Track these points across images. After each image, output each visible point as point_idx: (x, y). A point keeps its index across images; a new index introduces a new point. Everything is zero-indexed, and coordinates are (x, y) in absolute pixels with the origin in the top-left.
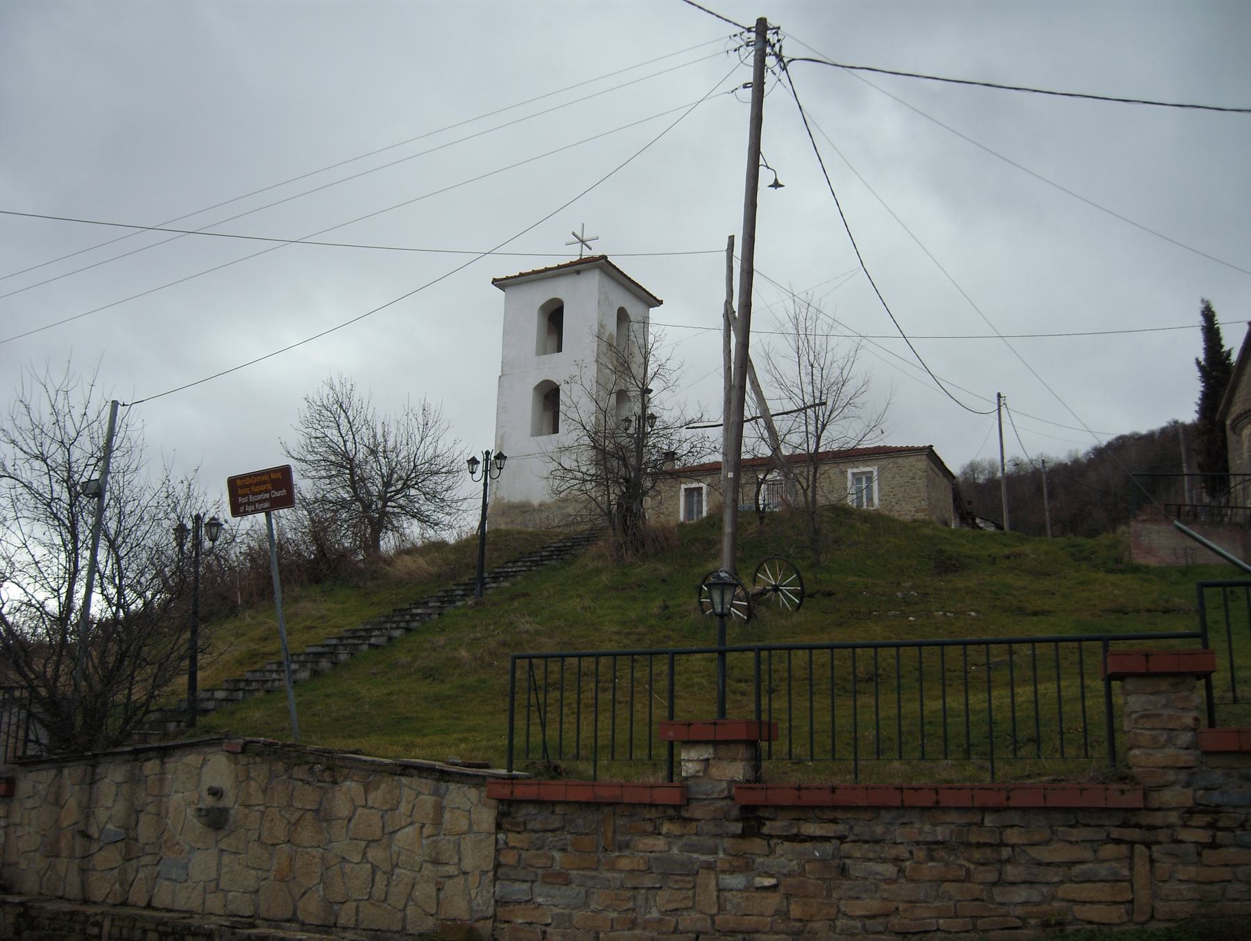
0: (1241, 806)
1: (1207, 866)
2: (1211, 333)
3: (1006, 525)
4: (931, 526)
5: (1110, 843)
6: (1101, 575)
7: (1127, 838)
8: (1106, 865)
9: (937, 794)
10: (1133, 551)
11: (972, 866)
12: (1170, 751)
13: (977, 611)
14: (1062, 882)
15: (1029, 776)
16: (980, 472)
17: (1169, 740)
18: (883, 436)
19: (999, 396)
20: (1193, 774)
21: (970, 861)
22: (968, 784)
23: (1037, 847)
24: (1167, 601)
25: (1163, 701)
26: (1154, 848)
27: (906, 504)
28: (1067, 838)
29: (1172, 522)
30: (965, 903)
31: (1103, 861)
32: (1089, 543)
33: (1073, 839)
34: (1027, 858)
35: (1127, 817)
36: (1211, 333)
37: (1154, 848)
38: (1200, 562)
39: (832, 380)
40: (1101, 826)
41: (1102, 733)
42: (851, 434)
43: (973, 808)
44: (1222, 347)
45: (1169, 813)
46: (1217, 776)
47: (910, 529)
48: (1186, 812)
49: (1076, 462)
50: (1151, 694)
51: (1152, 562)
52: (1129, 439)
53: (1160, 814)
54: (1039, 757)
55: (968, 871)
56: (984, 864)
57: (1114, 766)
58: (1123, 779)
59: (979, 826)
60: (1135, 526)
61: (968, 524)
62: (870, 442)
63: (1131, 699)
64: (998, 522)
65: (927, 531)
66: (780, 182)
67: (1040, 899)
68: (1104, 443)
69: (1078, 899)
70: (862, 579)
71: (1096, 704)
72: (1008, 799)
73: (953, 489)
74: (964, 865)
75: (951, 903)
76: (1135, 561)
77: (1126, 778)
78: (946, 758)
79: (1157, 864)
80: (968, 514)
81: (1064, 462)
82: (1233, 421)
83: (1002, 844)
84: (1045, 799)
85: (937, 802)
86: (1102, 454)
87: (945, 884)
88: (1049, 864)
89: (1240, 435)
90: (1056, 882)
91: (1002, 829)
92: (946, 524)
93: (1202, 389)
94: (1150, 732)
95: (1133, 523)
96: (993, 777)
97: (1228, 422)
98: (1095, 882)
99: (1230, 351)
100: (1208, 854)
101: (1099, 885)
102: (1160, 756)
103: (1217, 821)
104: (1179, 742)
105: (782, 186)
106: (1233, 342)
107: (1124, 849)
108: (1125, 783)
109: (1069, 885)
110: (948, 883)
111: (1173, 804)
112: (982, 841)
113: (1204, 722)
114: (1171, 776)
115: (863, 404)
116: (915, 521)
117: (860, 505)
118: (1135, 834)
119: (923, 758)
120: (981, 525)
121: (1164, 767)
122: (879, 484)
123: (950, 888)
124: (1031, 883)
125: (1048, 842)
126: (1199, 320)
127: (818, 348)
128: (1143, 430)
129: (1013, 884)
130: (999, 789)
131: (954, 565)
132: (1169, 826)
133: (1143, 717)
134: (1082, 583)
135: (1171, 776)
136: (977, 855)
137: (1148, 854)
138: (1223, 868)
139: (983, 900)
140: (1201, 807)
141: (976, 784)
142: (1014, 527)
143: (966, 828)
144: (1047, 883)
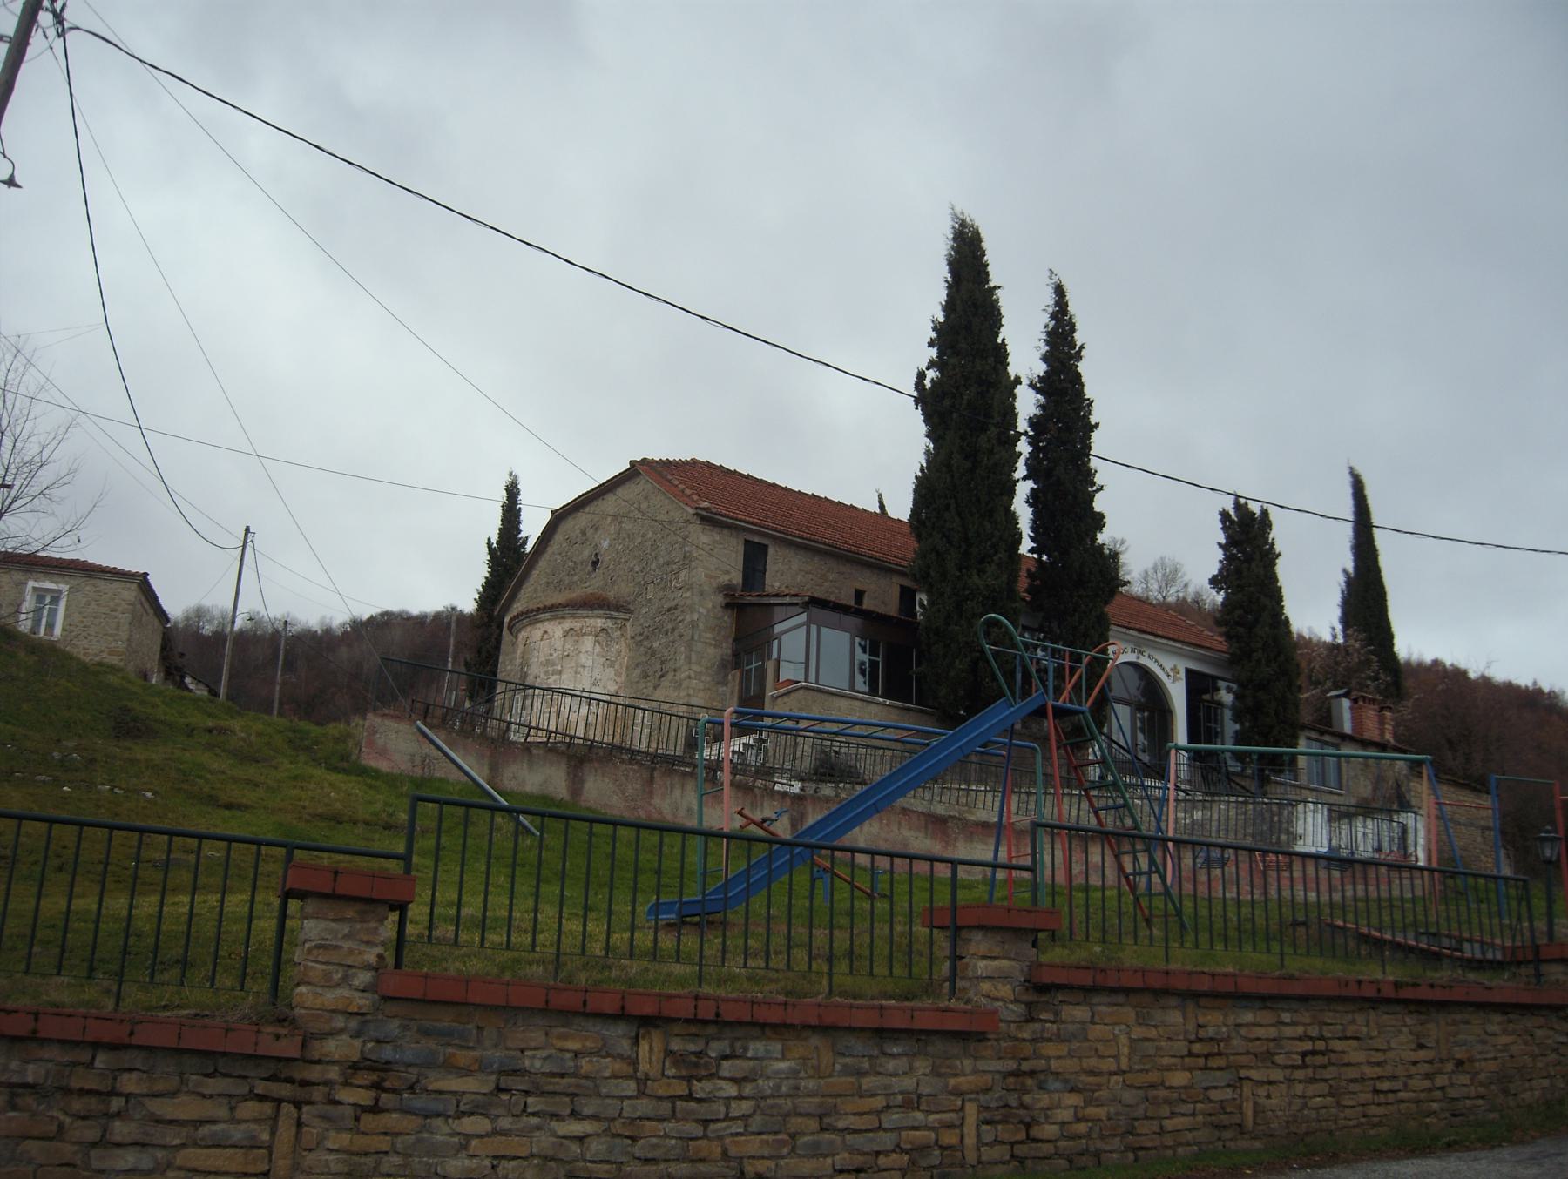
0: (416, 1065)
1: (363, 1133)
2: (511, 513)
3: (223, 691)
4: (120, 675)
5: (252, 1099)
6: (319, 772)
7: (275, 1095)
8: (243, 1127)
9: (36, 1020)
10: (363, 749)
11: (68, 1120)
12: (344, 992)
13: (155, 793)
14: (183, 1146)
15: (165, 1007)
16: (207, 621)
17: (345, 978)
18: (80, 545)
19: (247, 530)
20: (366, 1021)
21: (66, 1113)
22: (82, 1010)
23: (159, 1100)
24: (391, 815)
25: (346, 931)
26: (305, 1109)
27: (98, 641)
28: (200, 1090)
29: (415, 722)
30: (50, 1168)
31: (239, 1122)
32: (315, 730)
33: (207, 1092)
34: (144, 1112)
35: (278, 1071)
36: (511, 513)
37: (305, 1109)
38: (437, 774)
39: (27, 459)
40: (245, 1077)
41: (268, 962)
42: (36, 534)
43: (82, 1042)
44: (520, 532)
45: (330, 1067)
46: (393, 1027)
47: (92, 673)
48: (350, 1067)
49: (328, 631)
50: (334, 920)
51: (383, 766)
52: (396, 618)
53: (318, 1067)
54: (182, 984)
55: (61, 1127)
56: (84, 1118)
57: (274, 1004)
58: (281, 1021)
59: (88, 1067)
60: (372, 719)
61: (174, 683)
62: (60, 550)
63: (308, 924)
64: (213, 687)
65: (112, 679)
66: (18, 180)
67: (151, 1166)
68: (365, 617)
69: (200, 1169)
70: (9, 727)
71: (266, 926)
72: (131, 1034)
73: (164, 634)
74: (58, 1118)
75: (31, 1168)
76: (363, 762)
77: (284, 1020)
78: (59, 974)
79: (305, 1129)
80: (178, 669)
81: (314, 630)
82: (512, 619)
83: (113, 1093)
84: (179, 1038)
85: (35, 1032)
86: (361, 629)
87: (27, 1142)
88: (171, 1122)
89: (516, 638)
90: (176, 1146)
91: (117, 1073)
92: (145, 676)
93: (488, 575)
94: (324, 967)
95: (370, 716)
96: (117, 1004)
97: (507, 620)
98: (225, 1147)
99: (527, 538)
100: (368, 1121)
101: (231, 1151)
102: (331, 997)
103: (384, 1080)
104: (356, 982)
105: (19, 186)
106: (532, 527)
107: (267, 1108)
108: (284, 1027)
109: (192, 1150)
110: (31, 1141)
111: (337, 1057)
112: (87, 1087)
113: (390, 961)
114: (339, 1022)
115: (62, 499)
116: (100, 664)
117: (34, 630)
118: (285, 1090)
119: (27, 972)
120: (191, 686)
121: (334, 1011)
122: (67, 609)
123: (33, 1147)
124: (144, 1145)
125: (174, 1094)
126: (502, 495)
127: (17, 411)
128: (415, 609)
129: (119, 1145)
130: (122, 1021)
131: (138, 729)
132: (327, 1083)
133: (318, 947)
134: (295, 778)
135: (339, 1022)
136: (77, 1105)
137: (296, 1115)
138: (382, 1137)
139: (74, 1166)
140: (369, 1063)
141: (93, 1011)
142: (230, 697)
143: (68, 1068)
144: (164, 1147)
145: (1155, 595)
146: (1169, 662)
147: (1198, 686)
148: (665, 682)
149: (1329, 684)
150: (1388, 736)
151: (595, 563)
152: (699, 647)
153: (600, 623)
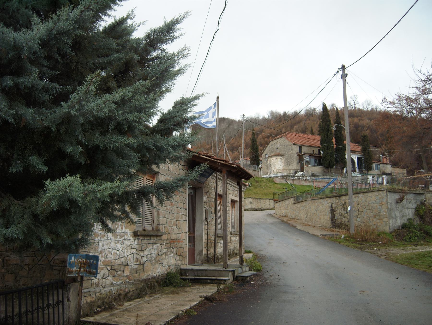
145: (366, 109)
146: (354, 156)
147: (359, 159)
148: (291, 165)
149: (380, 154)
150: (388, 162)
151: (277, 148)
152: (295, 161)
153: (280, 157)
